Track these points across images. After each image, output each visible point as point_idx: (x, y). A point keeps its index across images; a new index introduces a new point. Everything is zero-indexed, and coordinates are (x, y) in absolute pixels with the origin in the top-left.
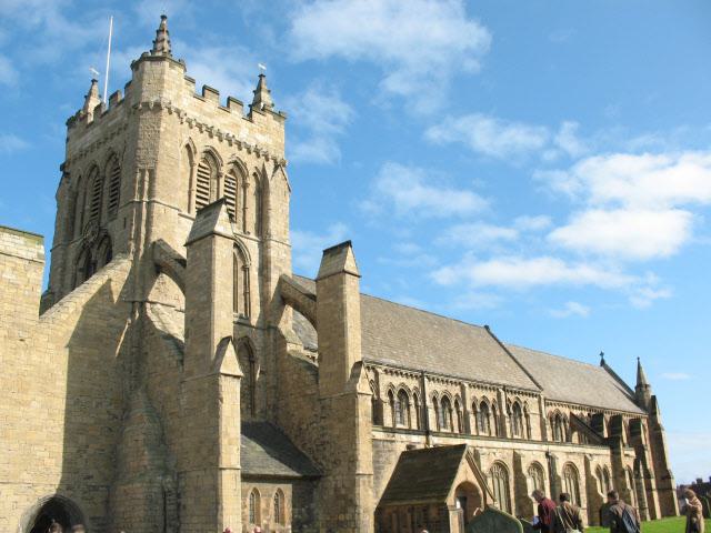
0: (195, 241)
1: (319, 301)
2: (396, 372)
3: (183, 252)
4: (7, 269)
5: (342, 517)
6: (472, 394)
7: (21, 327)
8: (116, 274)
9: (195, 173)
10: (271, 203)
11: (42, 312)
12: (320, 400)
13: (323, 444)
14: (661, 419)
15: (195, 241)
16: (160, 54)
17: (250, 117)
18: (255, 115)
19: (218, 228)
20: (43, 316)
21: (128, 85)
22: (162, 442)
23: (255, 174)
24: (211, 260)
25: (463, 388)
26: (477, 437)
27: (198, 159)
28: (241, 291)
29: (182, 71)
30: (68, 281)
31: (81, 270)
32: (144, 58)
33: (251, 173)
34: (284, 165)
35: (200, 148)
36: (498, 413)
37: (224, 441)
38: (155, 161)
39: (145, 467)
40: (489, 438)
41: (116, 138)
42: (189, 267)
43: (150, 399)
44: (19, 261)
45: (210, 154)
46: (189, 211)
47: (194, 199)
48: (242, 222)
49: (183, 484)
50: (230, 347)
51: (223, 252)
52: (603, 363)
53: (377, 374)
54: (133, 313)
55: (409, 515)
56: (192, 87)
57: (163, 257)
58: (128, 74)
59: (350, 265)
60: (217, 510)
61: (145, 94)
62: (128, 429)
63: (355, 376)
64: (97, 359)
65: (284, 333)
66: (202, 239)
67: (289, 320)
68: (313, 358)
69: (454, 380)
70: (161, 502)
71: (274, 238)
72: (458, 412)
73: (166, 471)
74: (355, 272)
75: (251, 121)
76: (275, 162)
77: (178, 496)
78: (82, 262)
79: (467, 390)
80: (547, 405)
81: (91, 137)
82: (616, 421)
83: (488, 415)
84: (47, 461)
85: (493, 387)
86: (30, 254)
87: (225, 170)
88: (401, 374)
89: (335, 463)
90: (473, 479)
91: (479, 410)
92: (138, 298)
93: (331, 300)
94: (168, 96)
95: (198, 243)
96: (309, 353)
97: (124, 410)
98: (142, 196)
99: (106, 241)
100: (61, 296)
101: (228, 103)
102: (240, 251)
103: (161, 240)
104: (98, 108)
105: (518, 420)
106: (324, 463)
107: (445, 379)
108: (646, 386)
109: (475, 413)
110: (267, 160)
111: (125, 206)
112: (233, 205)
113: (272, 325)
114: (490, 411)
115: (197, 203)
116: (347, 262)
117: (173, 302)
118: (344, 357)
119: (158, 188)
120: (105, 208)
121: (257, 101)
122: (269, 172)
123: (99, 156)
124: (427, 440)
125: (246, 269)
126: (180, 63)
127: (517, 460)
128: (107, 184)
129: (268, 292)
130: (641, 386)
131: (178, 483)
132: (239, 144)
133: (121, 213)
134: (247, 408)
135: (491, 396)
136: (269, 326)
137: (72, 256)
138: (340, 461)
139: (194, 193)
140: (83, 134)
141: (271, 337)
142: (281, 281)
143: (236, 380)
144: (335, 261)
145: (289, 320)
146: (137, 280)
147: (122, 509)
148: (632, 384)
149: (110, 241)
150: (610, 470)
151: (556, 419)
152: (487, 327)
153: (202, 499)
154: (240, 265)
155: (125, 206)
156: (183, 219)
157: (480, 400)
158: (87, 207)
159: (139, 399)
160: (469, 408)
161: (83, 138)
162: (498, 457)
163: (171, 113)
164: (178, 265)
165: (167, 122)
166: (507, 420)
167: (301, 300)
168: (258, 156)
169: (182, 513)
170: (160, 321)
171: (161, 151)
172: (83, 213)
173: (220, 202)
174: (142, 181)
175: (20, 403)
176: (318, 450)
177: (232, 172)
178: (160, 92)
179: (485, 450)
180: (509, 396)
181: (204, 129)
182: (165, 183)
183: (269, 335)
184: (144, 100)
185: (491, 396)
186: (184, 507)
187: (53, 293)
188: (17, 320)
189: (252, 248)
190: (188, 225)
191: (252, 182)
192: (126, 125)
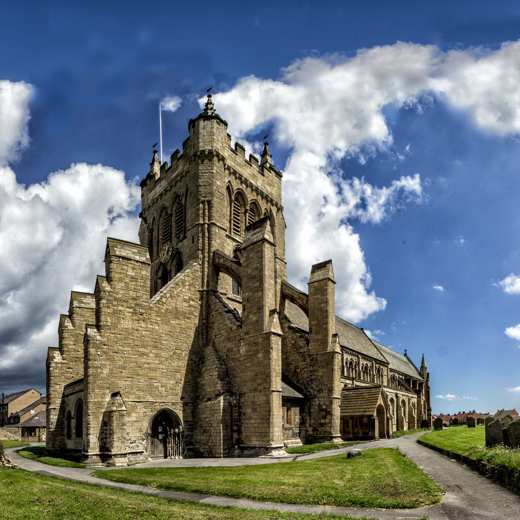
5: (323, 421)
12: (309, 355)
13: (311, 380)
14: (430, 384)
22: (226, 375)
24: (262, 258)
31: (160, 278)
38: (212, 194)
39: (219, 390)
41: (179, 184)
43: (217, 351)
49: (243, 401)
52: (405, 355)
55: (351, 421)
57: (222, 260)
60: (269, 415)
61: (201, 144)
62: (203, 370)
70: (229, 411)
72: (356, 370)
77: (240, 408)
78: (160, 274)
80: (390, 371)
82: (415, 382)
84: (160, 388)
86: (142, 258)
89: (319, 391)
90: (382, 404)
93: (319, 296)
97: (200, 359)
98: (204, 220)
99: (177, 256)
101: (250, 159)
106: (311, 391)
108: (426, 368)
118: (326, 330)
123: (167, 200)
124: (353, 382)
130: (423, 367)
131: (239, 400)
133: (189, 234)
138: (322, 390)
140: (155, 187)
147: (205, 416)
148: (419, 367)
150: (416, 405)
151: (393, 378)
153: (258, 409)
159: (209, 351)
161: (154, 191)
169: (243, 417)
172: (158, 242)
176: (308, 384)
178: (212, 142)
184: (200, 149)
186: (244, 414)
188: (138, 302)
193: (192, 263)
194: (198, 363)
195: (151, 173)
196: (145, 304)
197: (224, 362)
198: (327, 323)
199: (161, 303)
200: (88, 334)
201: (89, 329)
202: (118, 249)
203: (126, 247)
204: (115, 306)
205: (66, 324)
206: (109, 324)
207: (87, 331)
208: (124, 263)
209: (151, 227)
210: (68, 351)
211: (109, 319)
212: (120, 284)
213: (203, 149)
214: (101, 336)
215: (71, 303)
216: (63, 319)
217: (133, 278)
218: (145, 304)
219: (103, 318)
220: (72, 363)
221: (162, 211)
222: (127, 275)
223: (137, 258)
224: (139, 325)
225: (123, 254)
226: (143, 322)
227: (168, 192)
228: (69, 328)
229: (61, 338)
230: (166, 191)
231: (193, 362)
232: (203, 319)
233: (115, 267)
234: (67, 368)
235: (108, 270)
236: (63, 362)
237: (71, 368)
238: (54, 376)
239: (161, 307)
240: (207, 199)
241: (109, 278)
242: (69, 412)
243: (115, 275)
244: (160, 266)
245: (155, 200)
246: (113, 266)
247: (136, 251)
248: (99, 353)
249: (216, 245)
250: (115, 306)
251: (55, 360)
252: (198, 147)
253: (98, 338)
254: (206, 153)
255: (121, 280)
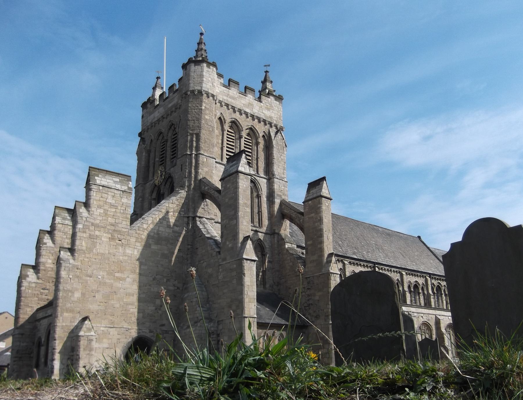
0: (226, 177)
1: (308, 215)
2: (357, 264)
3: (219, 185)
4: (109, 197)
6: (408, 279)
7: (119, 232)
8: (171, 206)
9: (225, 136)
10: (274, 155)
11: (132, 222)
13: (309, 305)
15: (226, 177)
16: (201, 59)
17: (259, 99)
18: (263, 97)
19: (240, 169)
20: (133, 225)
21: (180, 80)
23: (263, 136)
25: (402, 275)
26: (411, 306)
27: (227, 127)
28: (256, 210)
29: (215, 69)
30: (146, 205)
31: (154, 199)
32: (190, 61)
33: (261, 135)
34: (282, 130)
35: (228, 120)
36: (426, 292)
37: (246, 300)
38: (199, 127)
39: (197, 317)
40: (420, 307)
41: (174, 114)
42: (223, 194)
44: (116, 192)
45: (235, 124)
46: (222, 160)
47: (225, 152)
48: (256, 167)
50: (249, 242)
51: (244, 184)
53: (344, 264)
54: (188, 224)
56: (222, 80)
57: (206, 188)
58: (180, 73)
59: (325, 192)
61: (192, 85)
63: (329, 262)
64: (166, 252)
65: (283, 236)
66: (230, 177)
67: (287, 228)
68: (303, 253)
69: (395, 269)
71: (277, 177)
73: (210, 320)
74: (328, 196)
75: (261, 102)
76: (277, 128)
77: (218, 335)
79: (405, 276)
81: (157, 114)
83: (419, 293)
85: (422, 274)
87: (244, 134)
88: (360, 265)
91: (412, 290)
92: (191, 215)
93: (313, 215)
94: (206, 86)
95: (228, 178)
96: (299, 250)
97: (184, 284)
98: (192, 151)
99: (170, 180)
100: (142, 215)
102: (255, 185)
103: (205, 178)
104: (161, 96)
105: (440, 298)
107: (390, 269)
109: (410, 292)
110: (271, 127)
111: (182, 157)
112: (250, 156)
113: (277, 231)
114: (420, 291)
115: (227, 155)
116: (323, 190)
117: (213, 217)
118: (322, 250)
119: (202, 145)
120: (168, 159)
121: (264, 88)
122: (273, 135)
123: (163, 127)
125: (259, 197)
126: (214, 65)
127: (438, 322)
128: (169, 144)
129: (273, 211)
132: (253, 116)
133: (179, 162)
134: (261, 284)
135: (421, 281)
136: (273, 232)
137: (148, 191)
139: (225, 149)
140: (153, 112)
141: (276, 239)
142: (283, 203)
143: (253, 263)
144: (314, 191)
145: (287, 228)
146: (191, 204)
149: (172, 180)
152: (419, 237)
154: (255, 194)
155: (182, 157)
156: (217, 165)
157: (413, 283)
158: (157, 159)
160: (406, 289)
162: (425, 319)
163: (208, 97)
164: (216, 193)
165: (206, 103)
166: (432, 297)
167: (294, 215)
168: (265, 124)
170: (205, 228)
171: (203, 122)
172: (154, 163)
173: (241, 152)
174: (192, 141)
175: (120, 279)
177: (248, 135)
178: (201, 83)
179: (415, 314)
180: (433, 281)
181: (230, 107)
182: (205, 142)
183: (274, 238)
184: (191, 89)
185: (421, 281)
187: (137, 215)
188: (117, 228)
189: (263, 183)
190: (222, 168)
191: (261, 141)
192: (181, 105)
193: (178, 191)
194: (181, 289)
195: (151, 99)
196: (125, 230)
197: (206, 288)
198: (322, 242)
199: (141, 229)
200: (61, 256)
201: (62, 252)
202: (99, 178)
203: (107, 177)
204: (92, 231)
205: (45, 241)
206: (84, 248)
207: (60, 254)
208: (104, 191)
209: (148, 148)
210: (44, 270)
211: (84, 244)
212: (98, 211)
213: (194, 89)
214: (74, 259)
215: (54, 218)
216: (42, 235)
217: (112, 206)
218: (125, 230)
219: (78, 242)
220: (48, 284)
221: (159, 135)
222: (106, 202)
223: (118, 186)
224: (117, 250)
225: (104, 183)
226: (120, 247)
227: (165, 119)
228: (48, 245)
229: (38, 255)
230: (163, 117)
231: (176, 288)
232: (188, 245)
233: (95, 195)
234: (43, 289)
235: (88, 197)
236: (38, 281)
237: (48, 289)
238: (25, 297)
239: (142, 233)
240: (195, 132)
241: (87, 205)
242: (40, 338)
243: (93, 202)
244: (154, 188)
245: (153, 124)
246: (93, 194)
247: (118, 180)
248: (71, 277)
249: (203, 173)
250: (92, 231)
251: (28, 279)
252: (189, 87)
253: (72, 261)
254: (196, 93)
255: (99, 207)
